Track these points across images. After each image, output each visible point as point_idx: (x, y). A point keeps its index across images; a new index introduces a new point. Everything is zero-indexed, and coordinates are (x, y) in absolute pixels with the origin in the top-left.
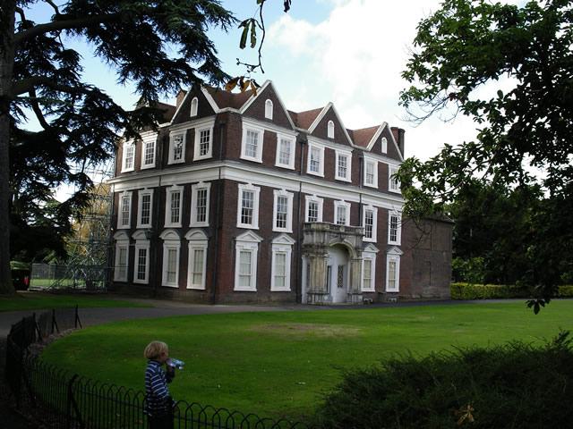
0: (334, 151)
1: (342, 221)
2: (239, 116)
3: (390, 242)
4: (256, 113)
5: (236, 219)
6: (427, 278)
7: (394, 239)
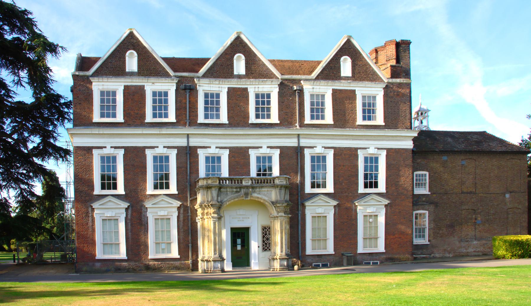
0: (354, 91)
5: (357, 184)
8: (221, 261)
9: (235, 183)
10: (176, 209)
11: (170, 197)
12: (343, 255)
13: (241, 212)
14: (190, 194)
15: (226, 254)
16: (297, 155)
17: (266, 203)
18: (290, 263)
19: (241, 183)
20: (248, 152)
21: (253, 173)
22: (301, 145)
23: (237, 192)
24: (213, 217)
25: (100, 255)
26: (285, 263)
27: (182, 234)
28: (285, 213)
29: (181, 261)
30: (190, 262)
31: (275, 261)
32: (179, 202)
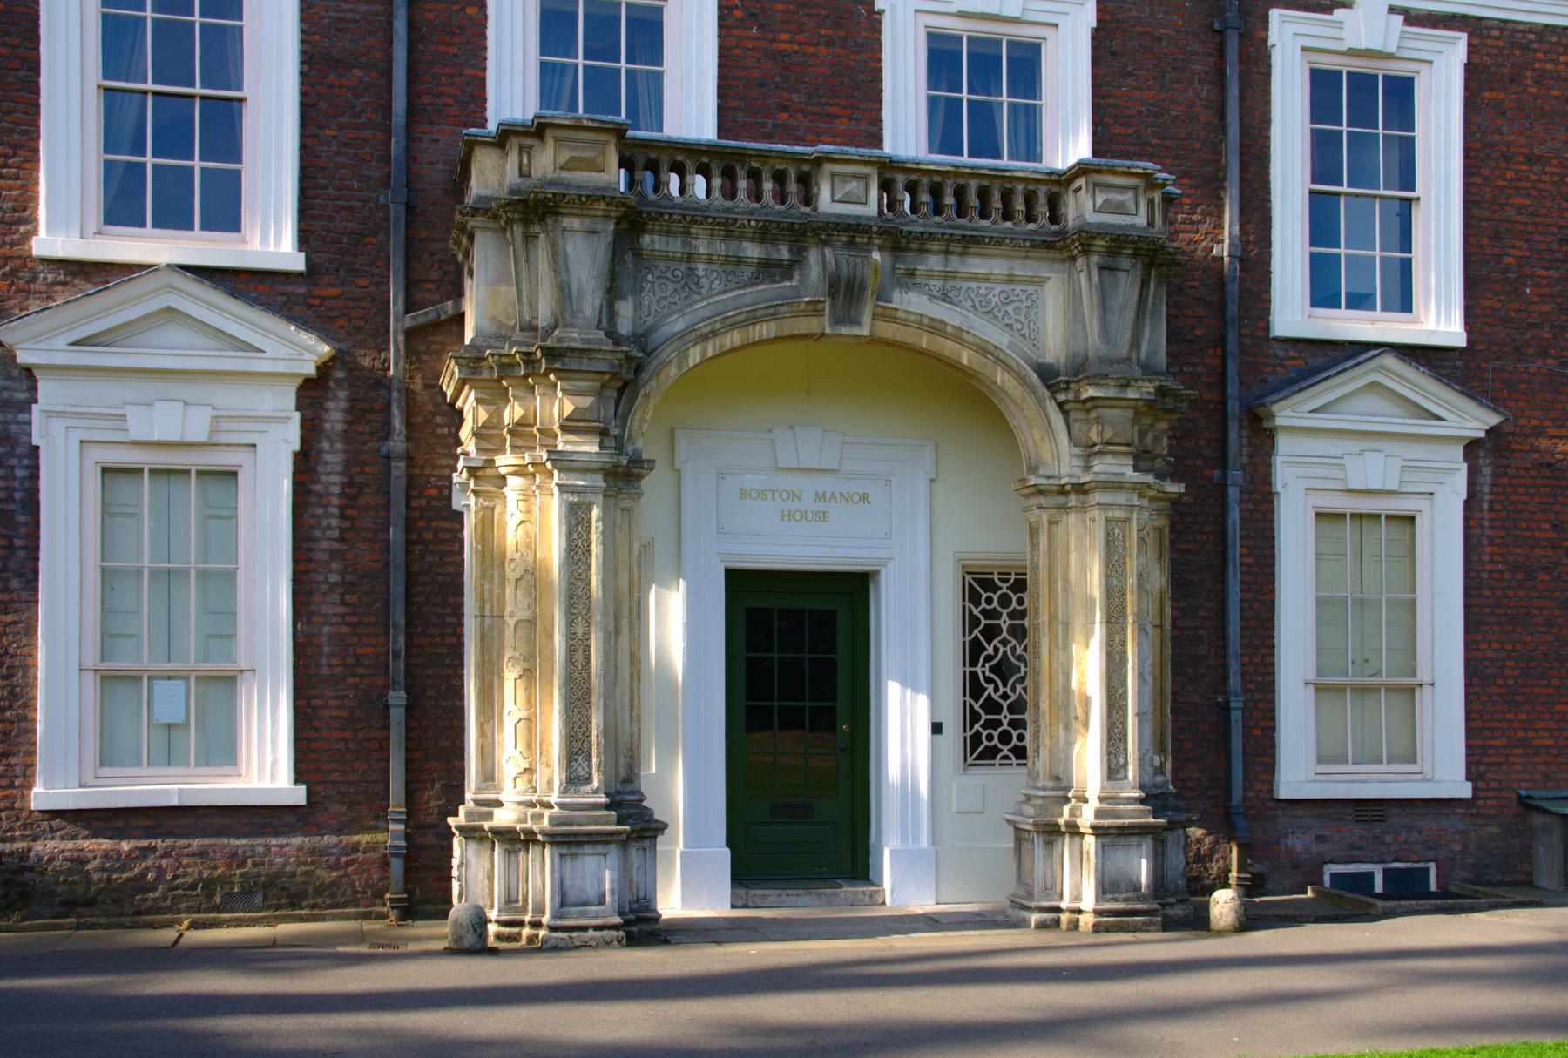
8: (624, 842)
9: (757, 195)
10: (285, 400)
11: (235, 293)
12: (1527, 805)
13: (810, 444)
14: (410, 285)
15: (686, 783)
16: (1221, 50)
17: (1000, 376)
18: (1176, 861)
19: (808, 199)
21: (905, 130)
23: (768, 269)
24: (562, 462)
26: (1143, 871)
27: (329, 607)
28: (1141, 459)
29: (319, 829)
30: (393, 834)
31: (1066, 847)
32: (308, 339)
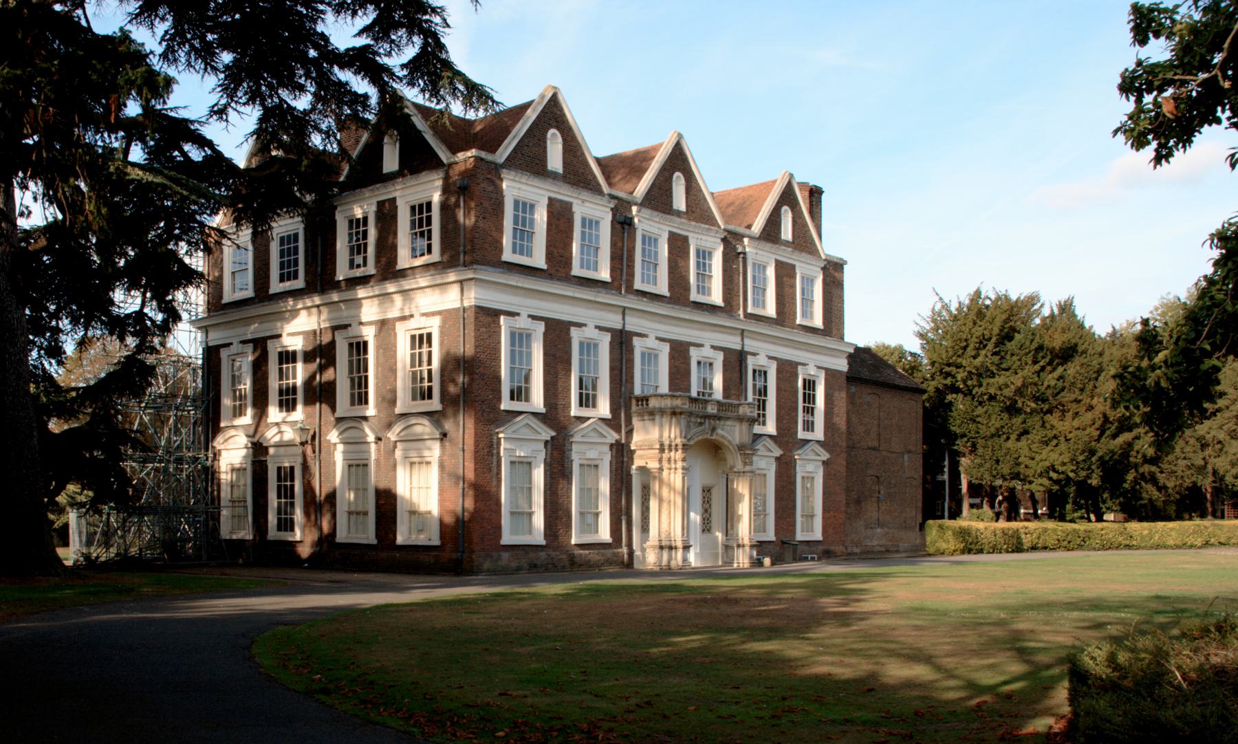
1: (706, 384)
2: (496, 169)
3: (801, 434)
4: (530, 160)
6: (871, 511)
7: (809, 426)
20: (688, 351)
22: (628, 328)
25: (507, 538)
